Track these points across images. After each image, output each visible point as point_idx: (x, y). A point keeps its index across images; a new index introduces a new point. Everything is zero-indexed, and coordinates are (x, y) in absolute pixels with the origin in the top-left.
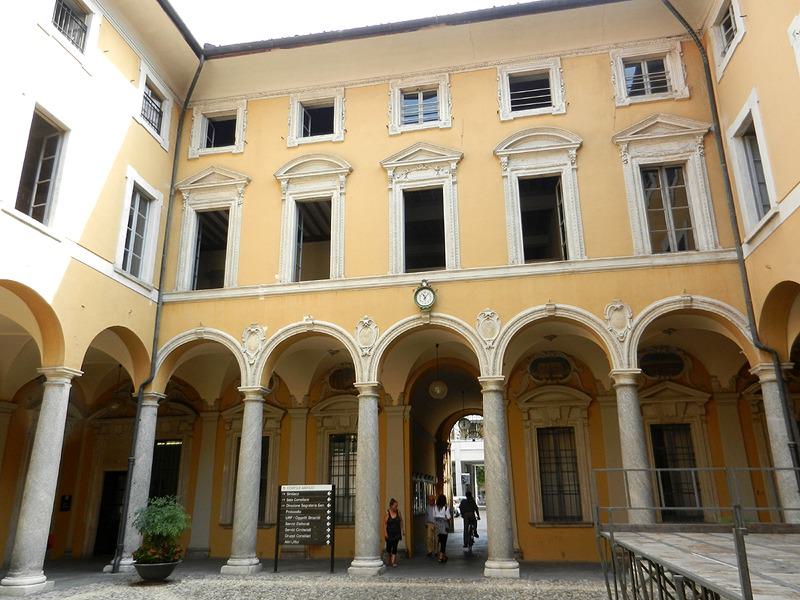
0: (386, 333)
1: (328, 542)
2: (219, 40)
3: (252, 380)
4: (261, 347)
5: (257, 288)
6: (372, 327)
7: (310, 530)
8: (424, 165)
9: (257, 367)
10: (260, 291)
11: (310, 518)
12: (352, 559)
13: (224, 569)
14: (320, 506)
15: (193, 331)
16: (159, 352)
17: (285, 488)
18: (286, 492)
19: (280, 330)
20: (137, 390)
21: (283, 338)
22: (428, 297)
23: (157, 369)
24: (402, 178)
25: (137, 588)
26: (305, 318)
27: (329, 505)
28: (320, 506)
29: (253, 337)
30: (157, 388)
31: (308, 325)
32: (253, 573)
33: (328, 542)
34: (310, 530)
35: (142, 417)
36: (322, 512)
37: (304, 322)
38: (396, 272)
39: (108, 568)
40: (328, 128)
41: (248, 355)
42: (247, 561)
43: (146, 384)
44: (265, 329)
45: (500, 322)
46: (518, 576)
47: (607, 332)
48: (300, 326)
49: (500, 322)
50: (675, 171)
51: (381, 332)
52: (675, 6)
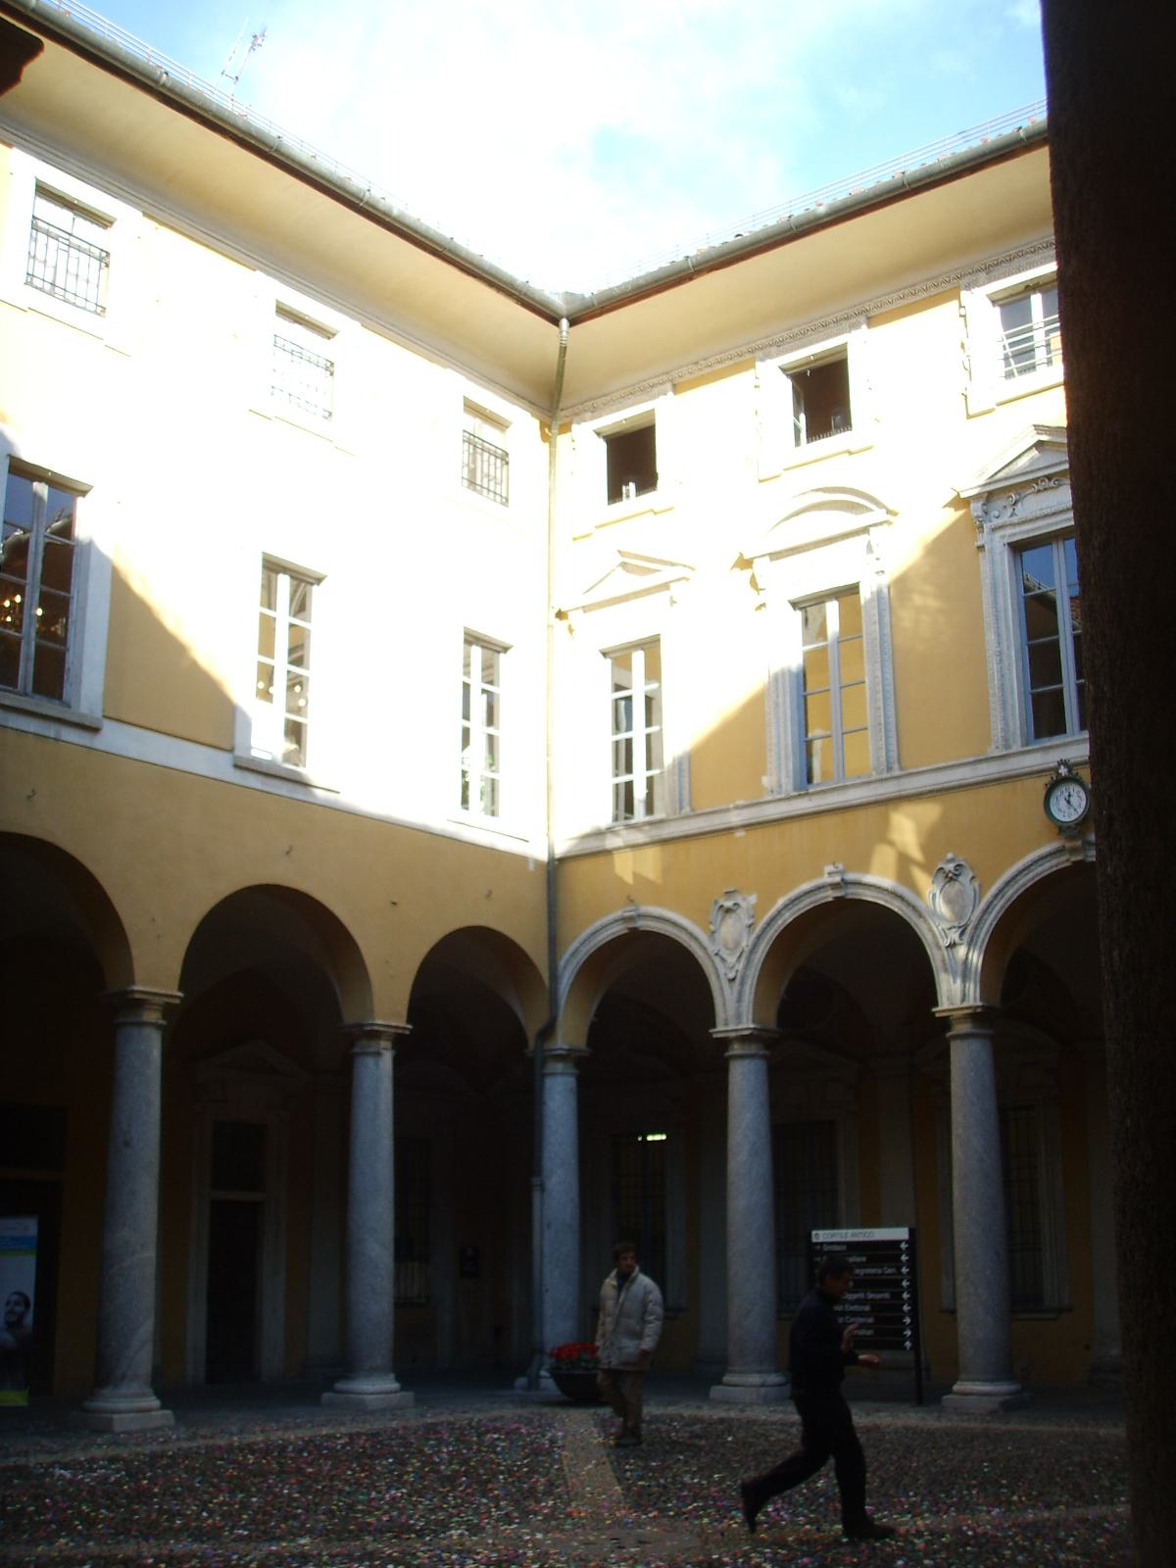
0: (993, 890)
1: (908, 1344)
2: (591, 285)
3: (736, 1009)
4: (746, 942)
5: (727, 810)
6: (965, 879)
7: (870, 1320)
8: (1049, 477)
9: (742, 983)
10: (735, 818)
11: (871, 1296)
12: (955, 1380)
13: (716, 1391)
14: (890, 1271)
15: (618, 914)
16: (562, 963)
17: (821, 1236)
18: (822, 1244)
19: (781, 902)
20: (532, 1043)
21: (788, 917)
22: (1074, 800)
23: (562, 1002)
24: (1005, 519)
25: (557, 1410)
26: (829, 868)
27: (904, 1270)
28: (890, 1271)
29: (730, 921)
30: (571, 1033)
31: (835, 886)
32: (766, 1401)
33: (908, 1344)
34: (870, 1320)
35: (547, 1096)
36: (894, 1284)
37: (826, 879)
38: (1007, 746)
39: (521, 1381)
40: (647, 480)
41: (723, 960)
42: (755, 1379)
43: (548, 1031)
44: (753, 899)
45: (976, 884)
46: (172, 1421)
47: (710, 957)
48: (819, 888)
49: (976, 884)
51: (983, 889)
52: (407, 341)
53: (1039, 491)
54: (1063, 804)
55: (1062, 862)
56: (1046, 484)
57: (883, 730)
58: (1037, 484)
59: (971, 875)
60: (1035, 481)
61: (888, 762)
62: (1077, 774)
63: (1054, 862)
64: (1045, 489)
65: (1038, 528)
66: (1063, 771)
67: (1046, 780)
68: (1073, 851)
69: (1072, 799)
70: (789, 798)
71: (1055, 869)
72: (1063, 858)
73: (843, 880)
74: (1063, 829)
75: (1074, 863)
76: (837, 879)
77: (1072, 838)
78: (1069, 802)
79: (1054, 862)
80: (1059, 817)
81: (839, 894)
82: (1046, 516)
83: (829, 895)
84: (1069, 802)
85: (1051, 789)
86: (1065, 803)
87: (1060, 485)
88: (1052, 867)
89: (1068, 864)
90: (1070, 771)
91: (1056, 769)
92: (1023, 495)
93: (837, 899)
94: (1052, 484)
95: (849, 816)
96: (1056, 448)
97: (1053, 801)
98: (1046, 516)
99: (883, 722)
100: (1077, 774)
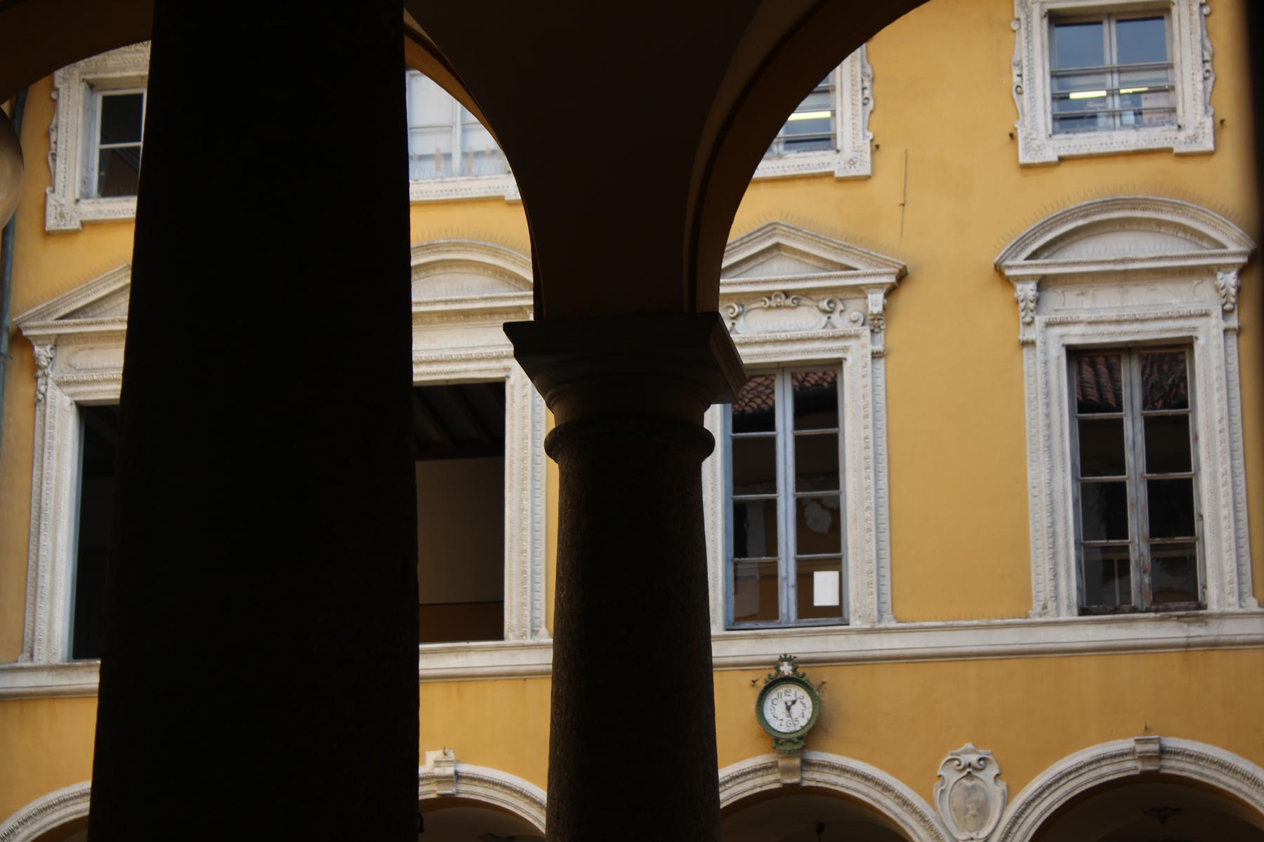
8: (787, 294)
22: (796, 709)
45: (1002, 786)
50: (1167, 363)
53: (770, 308)
54: (780, 709)
55: (769, 782)
56: (781, 300)
57: (529, 580)
58: (770, 298)
59: (996, 772)
60: (769, 295)
61: (533, 624)
62: (804, 675)
63: (758, 781)
64: (778, 307)
65: (765, 355)
66: (786, 669)
67: (762, 677)
68: (787, 771)
69: (793, 708)
70: (51, 668)
71: (758, 790)
72: (771, 778)
73: (456, 772)
74: (777, 741)
75: (785, 785)
76: (450, 771)
77: (790, 754)
78: (788, 708)
79: (749, 784)
80: (775, 724)
81: (1150, 767)
82: (776, 342)
83: (1132, 767)
84: (788, 708)
85: (776, 682)
86: (784, 706)
87: (798, 305)
88: (755, 787)
89: (777, 786)
90: (794, 670)
91: (776, 665)
92: (747, 308)
93: (1145, 774)
94: (789, 302)
95: (470, 689)
96: (797, 257)
97: (768, 704)
98: (776, 342)
99: (529, 570)
100: (804, 675)
